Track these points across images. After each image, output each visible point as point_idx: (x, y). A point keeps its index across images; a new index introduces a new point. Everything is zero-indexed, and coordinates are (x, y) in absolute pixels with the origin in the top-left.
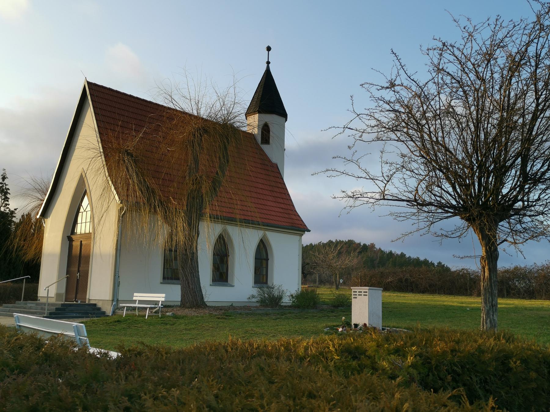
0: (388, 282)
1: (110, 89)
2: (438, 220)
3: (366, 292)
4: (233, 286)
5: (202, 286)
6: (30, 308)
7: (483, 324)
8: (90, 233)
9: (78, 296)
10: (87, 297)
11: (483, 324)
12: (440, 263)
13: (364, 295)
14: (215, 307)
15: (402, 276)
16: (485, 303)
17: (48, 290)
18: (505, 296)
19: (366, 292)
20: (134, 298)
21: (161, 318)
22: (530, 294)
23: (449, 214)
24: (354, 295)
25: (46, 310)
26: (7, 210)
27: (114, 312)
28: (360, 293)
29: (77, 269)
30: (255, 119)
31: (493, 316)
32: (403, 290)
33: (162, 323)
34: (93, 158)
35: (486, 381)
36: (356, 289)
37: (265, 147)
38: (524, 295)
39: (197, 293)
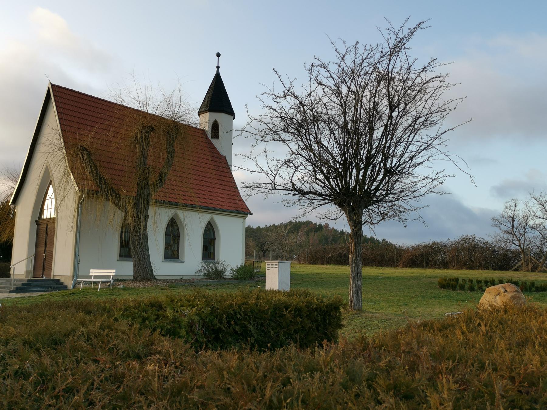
0: (330, 257)
1: (72, 91)
3: (277, 265)
4: (184, 262)
8: (54, 218)
10: (52, 273)
12: (384, 240)
13: (275, 267)
14: (163, 280)
15: (341, 251)
16: (352, 271)
17: (14, 268)
18: (425, 266)
19: (277, 265)
20: (91, 274)
21: (112, 290)
22: (445, 265)
23: (327, 201)
24: (268, 267)
25: (13, 284)
27: (74, 286)
28: (272, 266)
29: (43, 249)
31: (358, 281)
35: (262, 325)
36: (269, 263)
37: (214, 141)
38: (439, 265)
39: (147, 268)
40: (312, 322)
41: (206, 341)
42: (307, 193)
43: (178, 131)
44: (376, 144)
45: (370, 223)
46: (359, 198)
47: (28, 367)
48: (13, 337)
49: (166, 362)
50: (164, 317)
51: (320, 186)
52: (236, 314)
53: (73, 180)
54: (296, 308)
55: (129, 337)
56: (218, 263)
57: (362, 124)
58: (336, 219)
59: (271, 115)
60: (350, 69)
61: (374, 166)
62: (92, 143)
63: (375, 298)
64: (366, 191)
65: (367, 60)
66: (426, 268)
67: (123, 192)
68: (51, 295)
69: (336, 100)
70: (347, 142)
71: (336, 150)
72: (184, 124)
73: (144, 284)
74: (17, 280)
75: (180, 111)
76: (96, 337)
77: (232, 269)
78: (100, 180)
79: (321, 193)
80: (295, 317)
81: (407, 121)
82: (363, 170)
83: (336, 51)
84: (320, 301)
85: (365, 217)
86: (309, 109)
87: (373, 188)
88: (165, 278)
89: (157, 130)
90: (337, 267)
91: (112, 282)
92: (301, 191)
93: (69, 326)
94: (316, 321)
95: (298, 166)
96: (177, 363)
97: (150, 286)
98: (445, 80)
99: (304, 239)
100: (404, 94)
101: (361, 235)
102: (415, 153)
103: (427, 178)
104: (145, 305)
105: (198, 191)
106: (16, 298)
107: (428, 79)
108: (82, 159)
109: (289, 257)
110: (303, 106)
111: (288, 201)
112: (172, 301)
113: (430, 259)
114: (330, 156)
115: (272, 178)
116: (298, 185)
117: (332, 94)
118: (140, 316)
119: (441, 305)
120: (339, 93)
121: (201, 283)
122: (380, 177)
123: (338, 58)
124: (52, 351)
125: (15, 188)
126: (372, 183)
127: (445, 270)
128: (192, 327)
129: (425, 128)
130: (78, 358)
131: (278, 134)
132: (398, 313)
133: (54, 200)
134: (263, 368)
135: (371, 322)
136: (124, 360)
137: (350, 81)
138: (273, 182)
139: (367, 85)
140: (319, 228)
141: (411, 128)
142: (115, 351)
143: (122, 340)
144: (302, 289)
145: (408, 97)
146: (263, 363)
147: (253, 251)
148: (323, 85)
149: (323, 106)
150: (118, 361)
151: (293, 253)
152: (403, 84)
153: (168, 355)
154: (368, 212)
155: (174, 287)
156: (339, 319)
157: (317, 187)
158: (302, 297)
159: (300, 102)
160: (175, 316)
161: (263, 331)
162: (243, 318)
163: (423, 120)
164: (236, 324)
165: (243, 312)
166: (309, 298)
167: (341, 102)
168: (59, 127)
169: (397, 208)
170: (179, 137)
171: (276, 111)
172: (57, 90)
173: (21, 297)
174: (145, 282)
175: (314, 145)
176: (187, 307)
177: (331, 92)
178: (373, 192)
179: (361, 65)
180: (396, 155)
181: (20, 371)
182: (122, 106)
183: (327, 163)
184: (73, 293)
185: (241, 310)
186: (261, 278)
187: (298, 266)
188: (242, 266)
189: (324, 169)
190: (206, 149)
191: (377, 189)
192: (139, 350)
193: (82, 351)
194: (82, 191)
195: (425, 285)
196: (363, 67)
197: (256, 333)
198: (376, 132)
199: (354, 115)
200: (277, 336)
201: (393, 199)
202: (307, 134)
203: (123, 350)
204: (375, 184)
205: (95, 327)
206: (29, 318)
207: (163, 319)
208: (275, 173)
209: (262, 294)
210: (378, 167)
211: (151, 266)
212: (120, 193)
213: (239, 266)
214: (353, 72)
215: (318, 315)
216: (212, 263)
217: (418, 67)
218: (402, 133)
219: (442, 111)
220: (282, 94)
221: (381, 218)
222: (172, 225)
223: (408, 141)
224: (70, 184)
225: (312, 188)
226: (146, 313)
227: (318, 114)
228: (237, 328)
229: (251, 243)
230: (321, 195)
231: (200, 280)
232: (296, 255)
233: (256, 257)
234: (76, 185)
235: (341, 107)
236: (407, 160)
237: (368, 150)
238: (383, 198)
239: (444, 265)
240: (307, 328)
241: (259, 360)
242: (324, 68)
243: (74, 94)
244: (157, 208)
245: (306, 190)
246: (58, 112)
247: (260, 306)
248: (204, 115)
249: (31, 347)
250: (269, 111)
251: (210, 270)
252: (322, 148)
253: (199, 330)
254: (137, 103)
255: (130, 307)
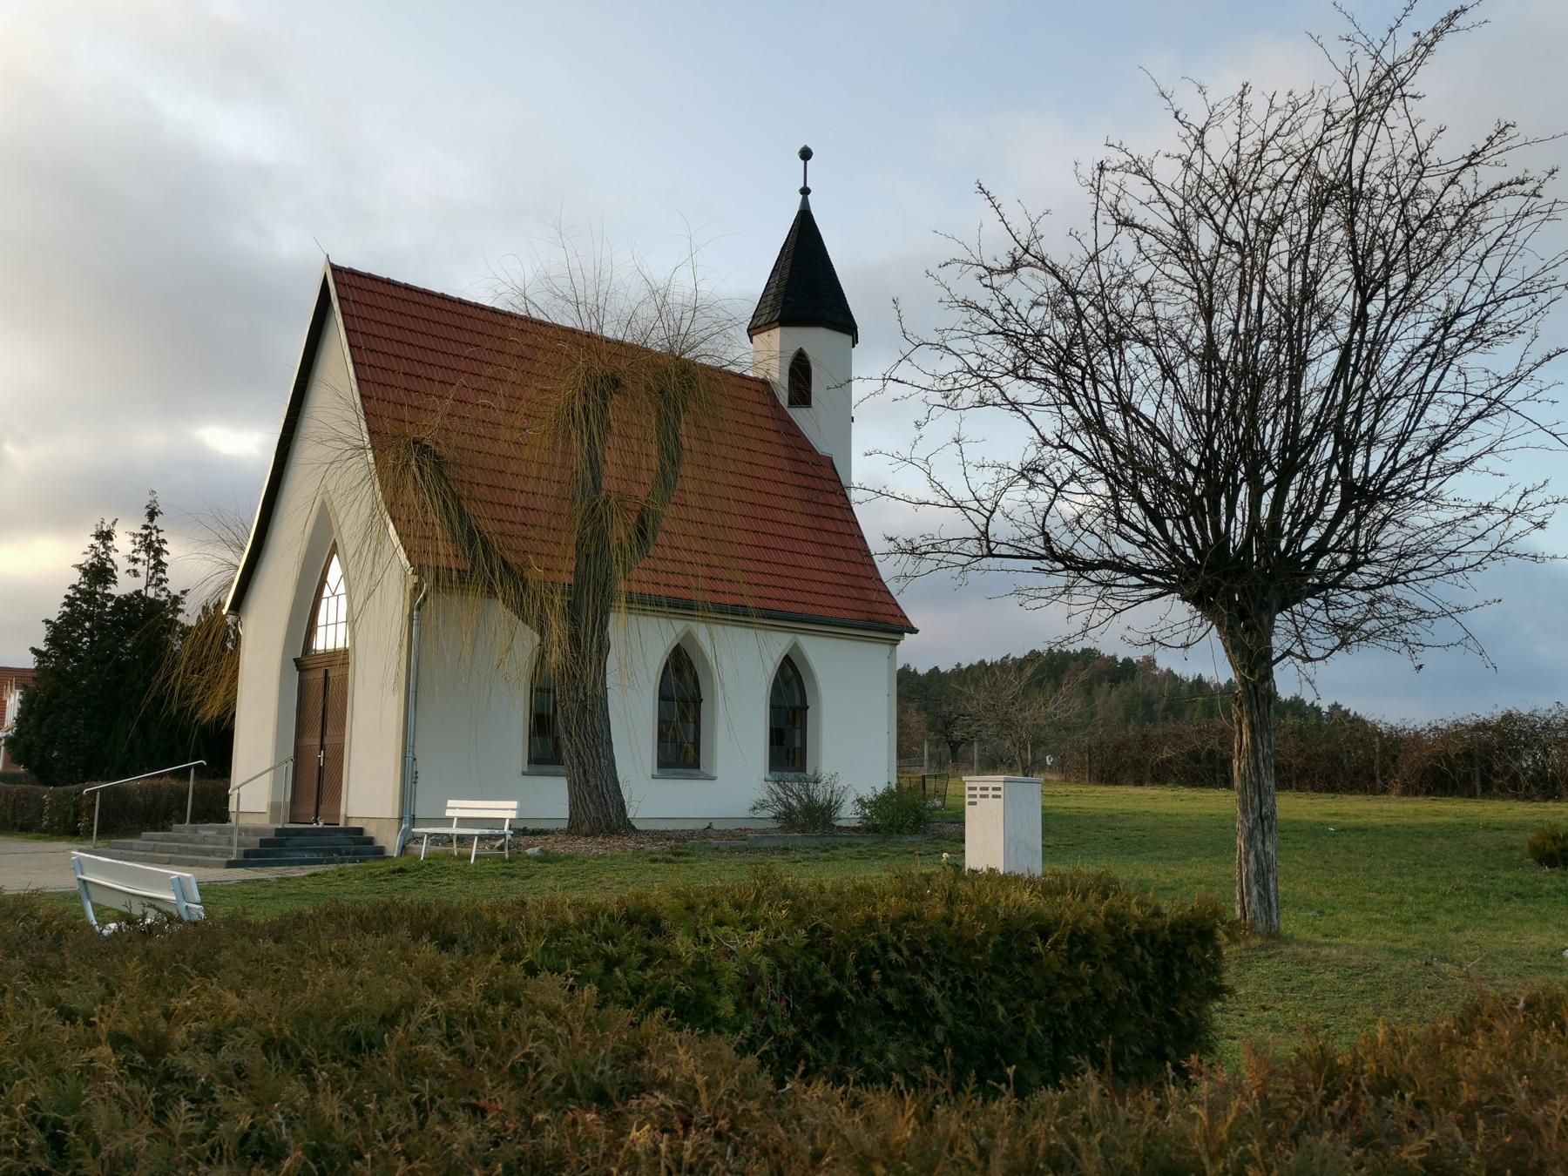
0: (1162, 761)
1: (389, 283)
2: (1130, 604)
3: (999, 789)
4: (714, 779)
5: (620, 779)
6: (204, 840)
7: (1240, 864)
8: (346, 651)
9: (322, 808)
10: (342, 811)
11: (1240, 864)
12: (1336, 707)
13: (994, 796)
14: (655, 832)
15: (1198, 744)
16: (1244, 811)
18: (1479, 790)
19: (999, 789)
20: (449, 813)
21: (510, 861)
23: (1157, 590)
24: (970, 796)
26: (164, 594)
28: (985, 793)
29: (317, 741)
30: (774, 339)
31: (1263, 843)
32: (1202, 780)
33: (504, 874)
34: (332, 463)
35: (967, 984)
37: (798, 415)
38: (1528, 788)
39: (607, 797)
40: (1127, 976)
41: (795, 1035)
42: (1091, 566)
43: (690, 387)
44: (1313, 406)
45: (1300, 657)
46: (1260, 578)
47: (278, 1125)
48: (235, 1025)
49: (685, 1117)
50: (668, 957)
51: (1133, 542)
52: (885, 951)
53: (396, 540)
54: (1073, 934)
55: (571, 1032)
56: (817, 782)
57: (1267, 342)
58: (1187, 646)
59: (975, 328)
60: (1223, 173)
61: (1306, 477)
62: (447, 430)
63: (1319, 894)
64: (1282, 555)
65: (1279, 140)
66: (1483, 797)
67: (535, 573)
68: (341, 875)
69: (1178, 272)
70: (1220, 404)
71: (1182, 431)
72: (709, 367)
73: (601, 844)
74: (246, 830)
75: (697, 326)
76: (474, 1027)
77: (860, 800)
78: (471, 538)
79: (1138, 564)
80: (1072, 961)
81: (1412, 331)
82: (1271, 491)
83: (1176, 117)
84: (1149, 911)
85: (1284, 638)
86: (1092, 303)
87: (1306, 545)
88: (661, 826)
89: (630, 385)
90: (1186, 792)
91: (509, 837)
92: (1072, 558)
93: (395, 990)
94: (1140, 975)
95: (1064, 483)
96: (721, 1122)
97: (617, 851)
98: (1540, 192)
99: (1077, 705)
100: (1406, 244)
101: (1271, 695)
102: (1444, 429)
103: (1488, 508)
104: (611, 918)
105: (752, 566)
106: (244, 882)
107: (1482, 191)
108: (419, 479)
109: (1034, 763)
110: (1073, 293)
111: (1031, 593)
112: (690, 908)
113: (1496, 768)
114: (1163, 450)
115: (980, 520)
116: (1064, 540)
117: (1167, 253)
118: (596, 955)
119: (1546, 920)
120: (1187, 250)
121: (767, 843)
122: (1330, 511)
123: (1184, 140)
124: (345, 1072)
125: (237, 568)
126: (1304, 531)
127: (1550, 804)
128: (752, 989)
129: (1480, 349)
130: (422, 1096)
131: (995, 385)
132: (1399, 946)
133: (343, 600)
134: (1005, 1156)
135: (1312, 976)
136: (557, 1104)
137: (1223, 211)
138: (985, 534)
139: (1281, 220)
140: (1123, 672)
141: (1432, 349)
142: (531, 1074)
143: (551, 1040)
144: (1089, 868)
145: (1417, 251)
146: (1003, 1143)
147: (920, 744)
148: (1136, 226)
149: (1137, 291)
150: (541, 1108)
151: (1043, 748)
152: (1402, 212)
153: (690, 1095)
154: (1294, 622)
155: (687, 855)
156: (1215, 970)
157: (1123, 548)
158: (1092, 897)
159: (1064, 284)
160: (699, 954)
161: (971, 1004)
162: (907, 961)
163: (1469, 323)
164: (887, 981)
165: (907, 943)
166: (1114, 901)
167: (1194, 277)
168: (355, 387)
169: (1390, 608)
170: (692, 405)
171: (990, 316)
172: (346, 281)
173: (258, 880)
174: (604, 838)
175: (1111, 414)
176: (736, 927)
177: (1161, 248)
178: (1307, 558)
179: (1260, 158)
180: (1381, 438)
181: (255, 1134)
182: (528, 320)
183: (1152, 471)
184: (401, 870)
185: (899, 939)
186: (952, 831)
187: (1062, 789)
188: (889, 790)
189: (1145, 489)
190: (774, 437)
191: (1320, 549)
192: (602, 1073)
193: (433, 1073)
194: (419, 570)
195: (1486, 853)
196: (1264, 164)
197: (951, 1011)
198: (1311, 370)
199: (1239, 316)
200: (1015, 1022)
201: (1375, 581)
202: (1088, 383)
203: (555, 1075)
204: (1314, 534)
205: (467, 996)
206: (281, 960)
207: (666, 962)
208: (988, 505)
209: (964, 888)
210: (1322, 477)
211: (618, 791)
212: (528, 575)
213: (880, 791)
214: (1233, 181)
215: (1147, 956)
216: (800, 781)
217: (1447, 151)
218: (1401, 366)
219: (1536, 289)
220: (1007, 262)
221: (1337, 641)
222: (678, 671)
223: (1420, 393)
224: (388, 553)
225: (1106, 550)
226: (615, 944)
227: (1122, 318)
228: (891, 995)
229: (914, 719)
230: (1136, 570)
231: (764, 832)
232: (1054, 756)
233: (930, 761)
234: (403, 556)
235: (1195, 294)
236: (1420, 452)
237: (1287, 424)
238: (1342, 577)
239: (1545, 788)
240: (1112, 997)
241: (987, 1126)
242: (1139, 172)
243: (393, 291)
244: (633, 617)
245: (1089, 555)
246: (350, 345)
247: (960, 923)
248: (764, 335)
249: (286, 1057)
250: (966, 316)
251: (794, 803)
252: (1137, 423)
253: (773, 998)
254: (571, 308)
255: (566, 926)
